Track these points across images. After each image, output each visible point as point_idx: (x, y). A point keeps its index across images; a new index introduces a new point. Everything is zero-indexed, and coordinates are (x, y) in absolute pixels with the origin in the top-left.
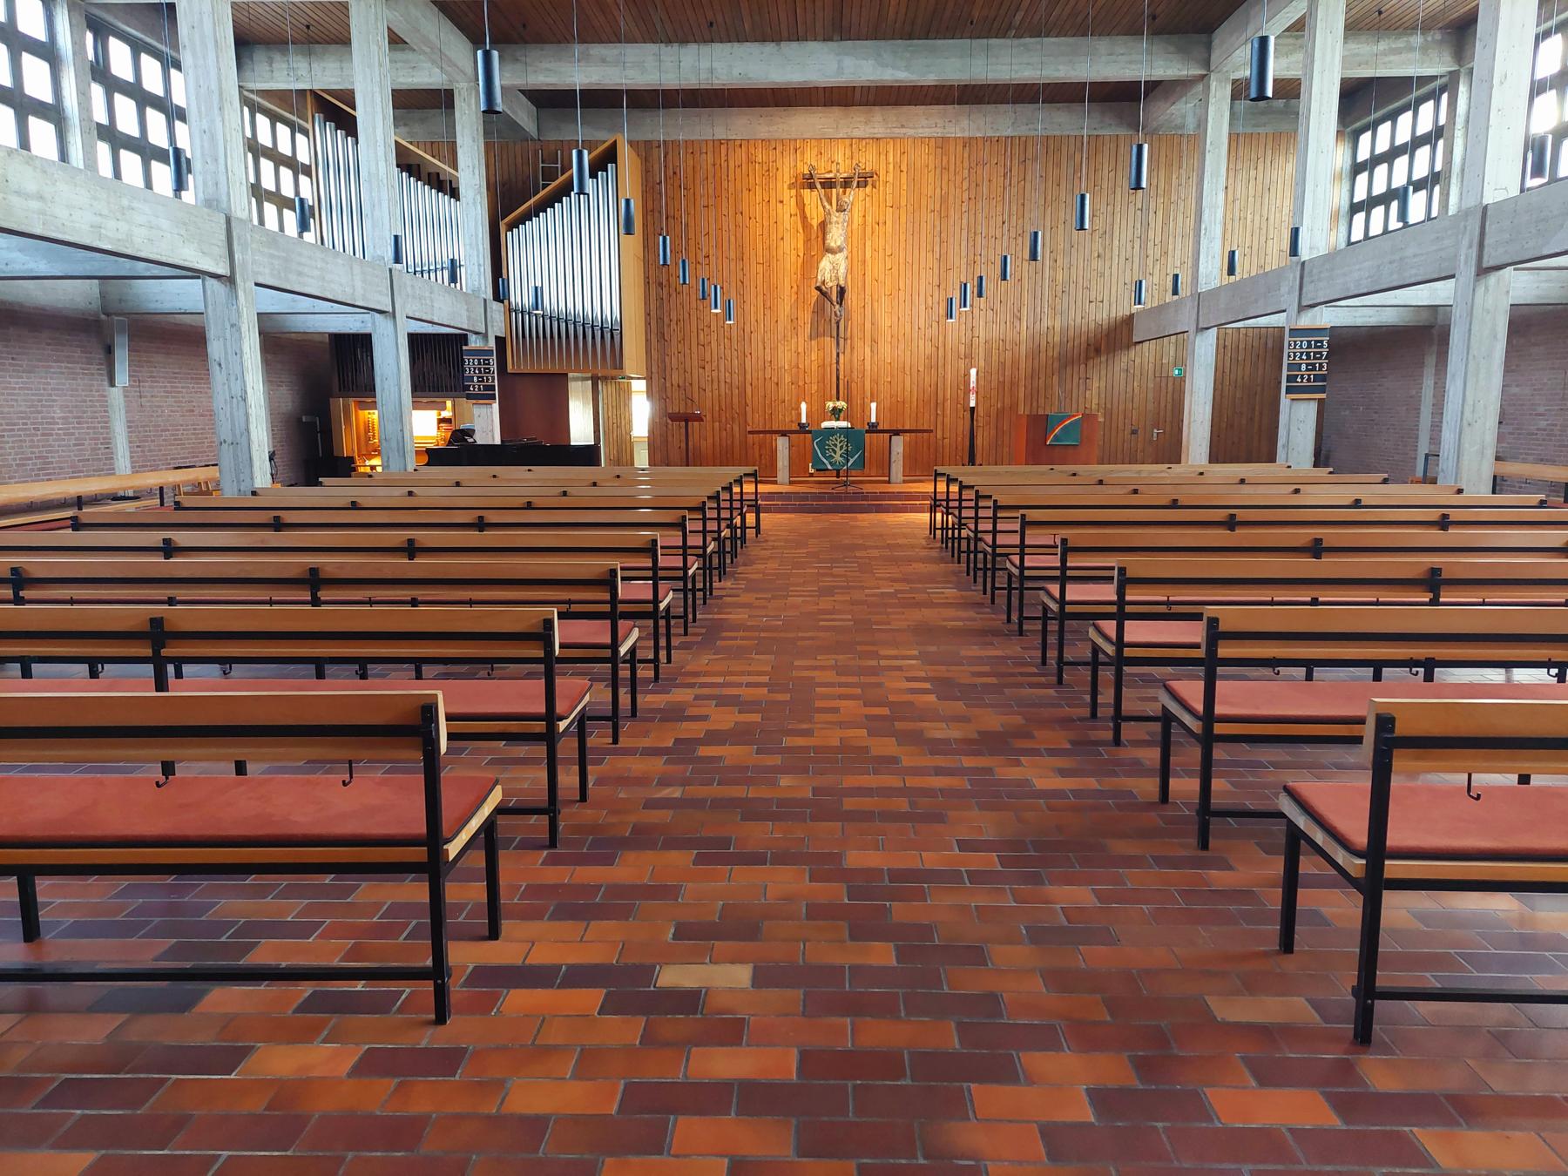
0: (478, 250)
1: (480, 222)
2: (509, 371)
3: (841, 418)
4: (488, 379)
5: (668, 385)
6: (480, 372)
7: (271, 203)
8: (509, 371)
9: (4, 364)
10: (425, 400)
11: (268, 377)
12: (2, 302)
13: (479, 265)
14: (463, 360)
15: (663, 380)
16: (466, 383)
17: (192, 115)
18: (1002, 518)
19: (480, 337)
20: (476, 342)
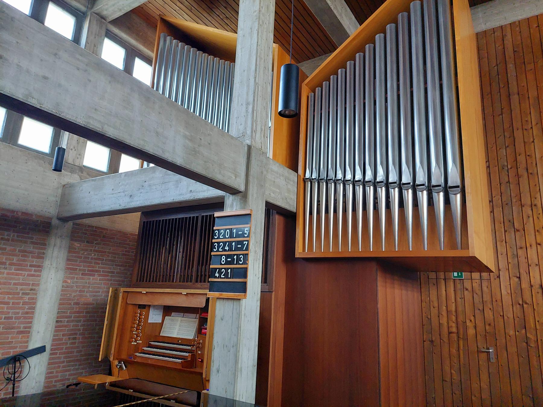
0: (248, 86)
1: (255, 52)
2: (297, 255)
3: (509, 27)
4: (239, 259)
5: (525, 285)
6: (230, 250)
7: (140, 82)
8: (297, 255)
9: (4, 263)
10: (184, 292)
11: (68, 264)
12: (3, 209)
13: (248, 104)
14: (213, 231)
15: (517, 280)
16: (211, 266)
17: (542, 244)
18: (224, 64)
19: (237, 198)
20: (232, 206)
